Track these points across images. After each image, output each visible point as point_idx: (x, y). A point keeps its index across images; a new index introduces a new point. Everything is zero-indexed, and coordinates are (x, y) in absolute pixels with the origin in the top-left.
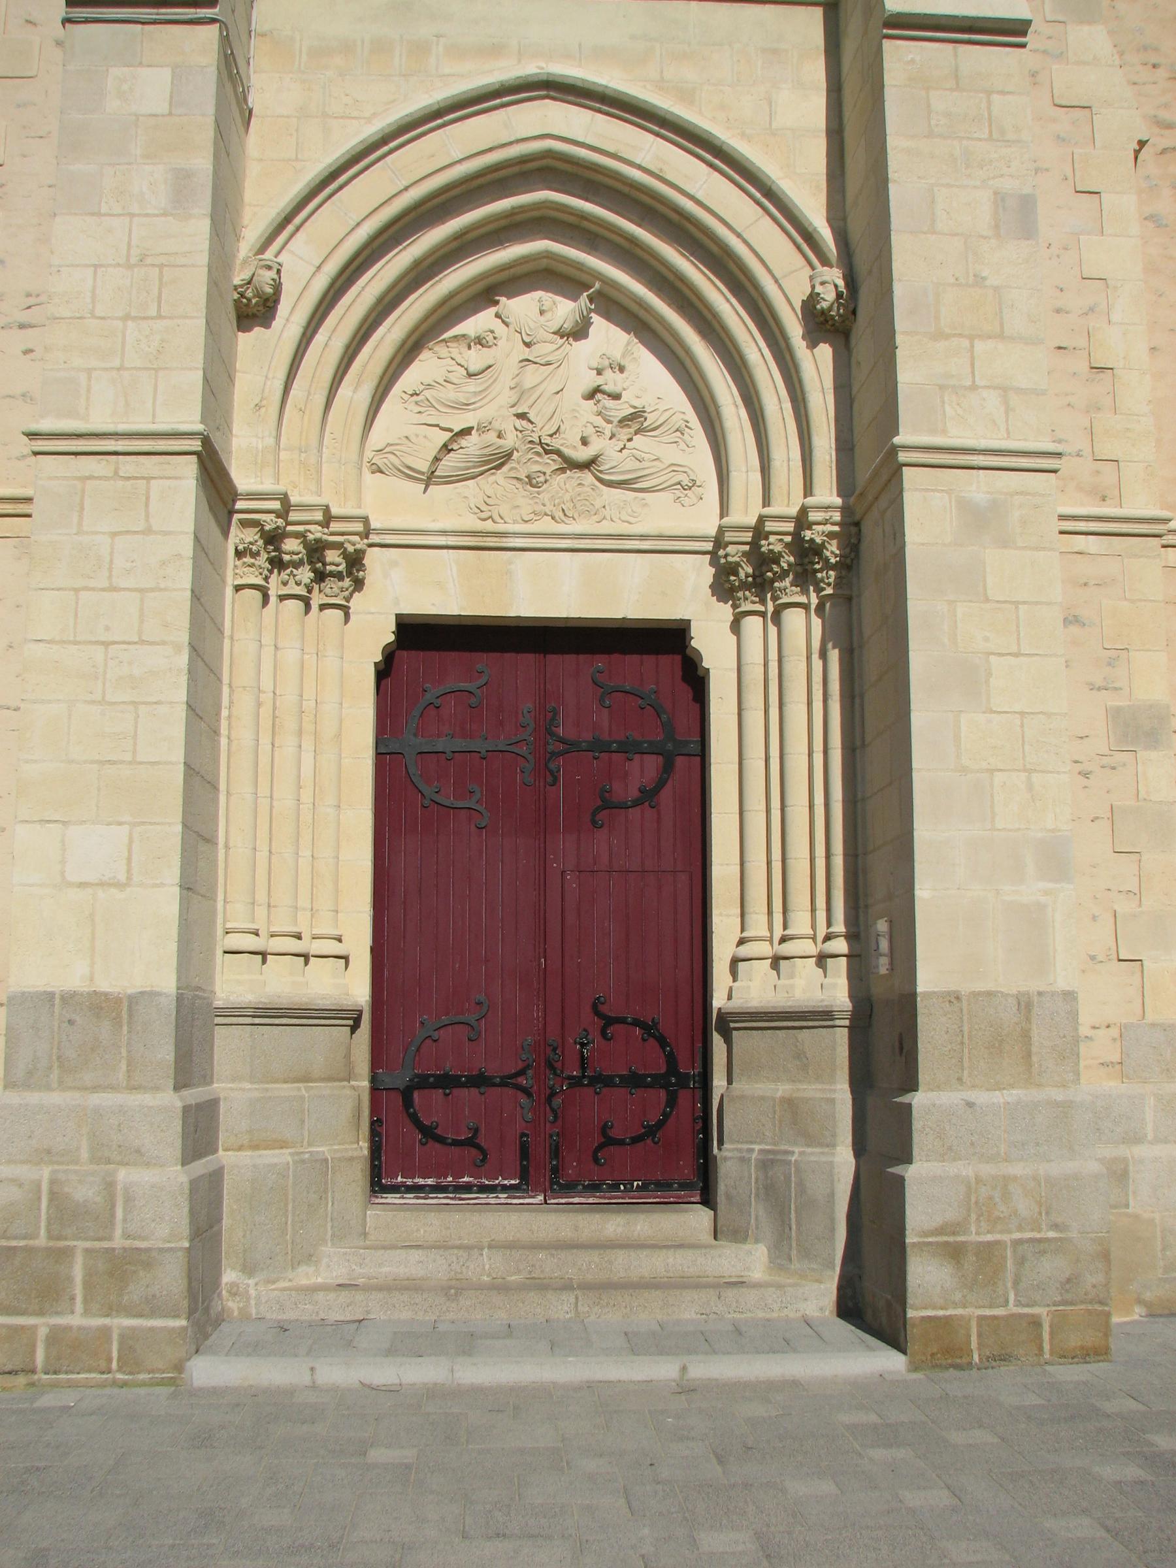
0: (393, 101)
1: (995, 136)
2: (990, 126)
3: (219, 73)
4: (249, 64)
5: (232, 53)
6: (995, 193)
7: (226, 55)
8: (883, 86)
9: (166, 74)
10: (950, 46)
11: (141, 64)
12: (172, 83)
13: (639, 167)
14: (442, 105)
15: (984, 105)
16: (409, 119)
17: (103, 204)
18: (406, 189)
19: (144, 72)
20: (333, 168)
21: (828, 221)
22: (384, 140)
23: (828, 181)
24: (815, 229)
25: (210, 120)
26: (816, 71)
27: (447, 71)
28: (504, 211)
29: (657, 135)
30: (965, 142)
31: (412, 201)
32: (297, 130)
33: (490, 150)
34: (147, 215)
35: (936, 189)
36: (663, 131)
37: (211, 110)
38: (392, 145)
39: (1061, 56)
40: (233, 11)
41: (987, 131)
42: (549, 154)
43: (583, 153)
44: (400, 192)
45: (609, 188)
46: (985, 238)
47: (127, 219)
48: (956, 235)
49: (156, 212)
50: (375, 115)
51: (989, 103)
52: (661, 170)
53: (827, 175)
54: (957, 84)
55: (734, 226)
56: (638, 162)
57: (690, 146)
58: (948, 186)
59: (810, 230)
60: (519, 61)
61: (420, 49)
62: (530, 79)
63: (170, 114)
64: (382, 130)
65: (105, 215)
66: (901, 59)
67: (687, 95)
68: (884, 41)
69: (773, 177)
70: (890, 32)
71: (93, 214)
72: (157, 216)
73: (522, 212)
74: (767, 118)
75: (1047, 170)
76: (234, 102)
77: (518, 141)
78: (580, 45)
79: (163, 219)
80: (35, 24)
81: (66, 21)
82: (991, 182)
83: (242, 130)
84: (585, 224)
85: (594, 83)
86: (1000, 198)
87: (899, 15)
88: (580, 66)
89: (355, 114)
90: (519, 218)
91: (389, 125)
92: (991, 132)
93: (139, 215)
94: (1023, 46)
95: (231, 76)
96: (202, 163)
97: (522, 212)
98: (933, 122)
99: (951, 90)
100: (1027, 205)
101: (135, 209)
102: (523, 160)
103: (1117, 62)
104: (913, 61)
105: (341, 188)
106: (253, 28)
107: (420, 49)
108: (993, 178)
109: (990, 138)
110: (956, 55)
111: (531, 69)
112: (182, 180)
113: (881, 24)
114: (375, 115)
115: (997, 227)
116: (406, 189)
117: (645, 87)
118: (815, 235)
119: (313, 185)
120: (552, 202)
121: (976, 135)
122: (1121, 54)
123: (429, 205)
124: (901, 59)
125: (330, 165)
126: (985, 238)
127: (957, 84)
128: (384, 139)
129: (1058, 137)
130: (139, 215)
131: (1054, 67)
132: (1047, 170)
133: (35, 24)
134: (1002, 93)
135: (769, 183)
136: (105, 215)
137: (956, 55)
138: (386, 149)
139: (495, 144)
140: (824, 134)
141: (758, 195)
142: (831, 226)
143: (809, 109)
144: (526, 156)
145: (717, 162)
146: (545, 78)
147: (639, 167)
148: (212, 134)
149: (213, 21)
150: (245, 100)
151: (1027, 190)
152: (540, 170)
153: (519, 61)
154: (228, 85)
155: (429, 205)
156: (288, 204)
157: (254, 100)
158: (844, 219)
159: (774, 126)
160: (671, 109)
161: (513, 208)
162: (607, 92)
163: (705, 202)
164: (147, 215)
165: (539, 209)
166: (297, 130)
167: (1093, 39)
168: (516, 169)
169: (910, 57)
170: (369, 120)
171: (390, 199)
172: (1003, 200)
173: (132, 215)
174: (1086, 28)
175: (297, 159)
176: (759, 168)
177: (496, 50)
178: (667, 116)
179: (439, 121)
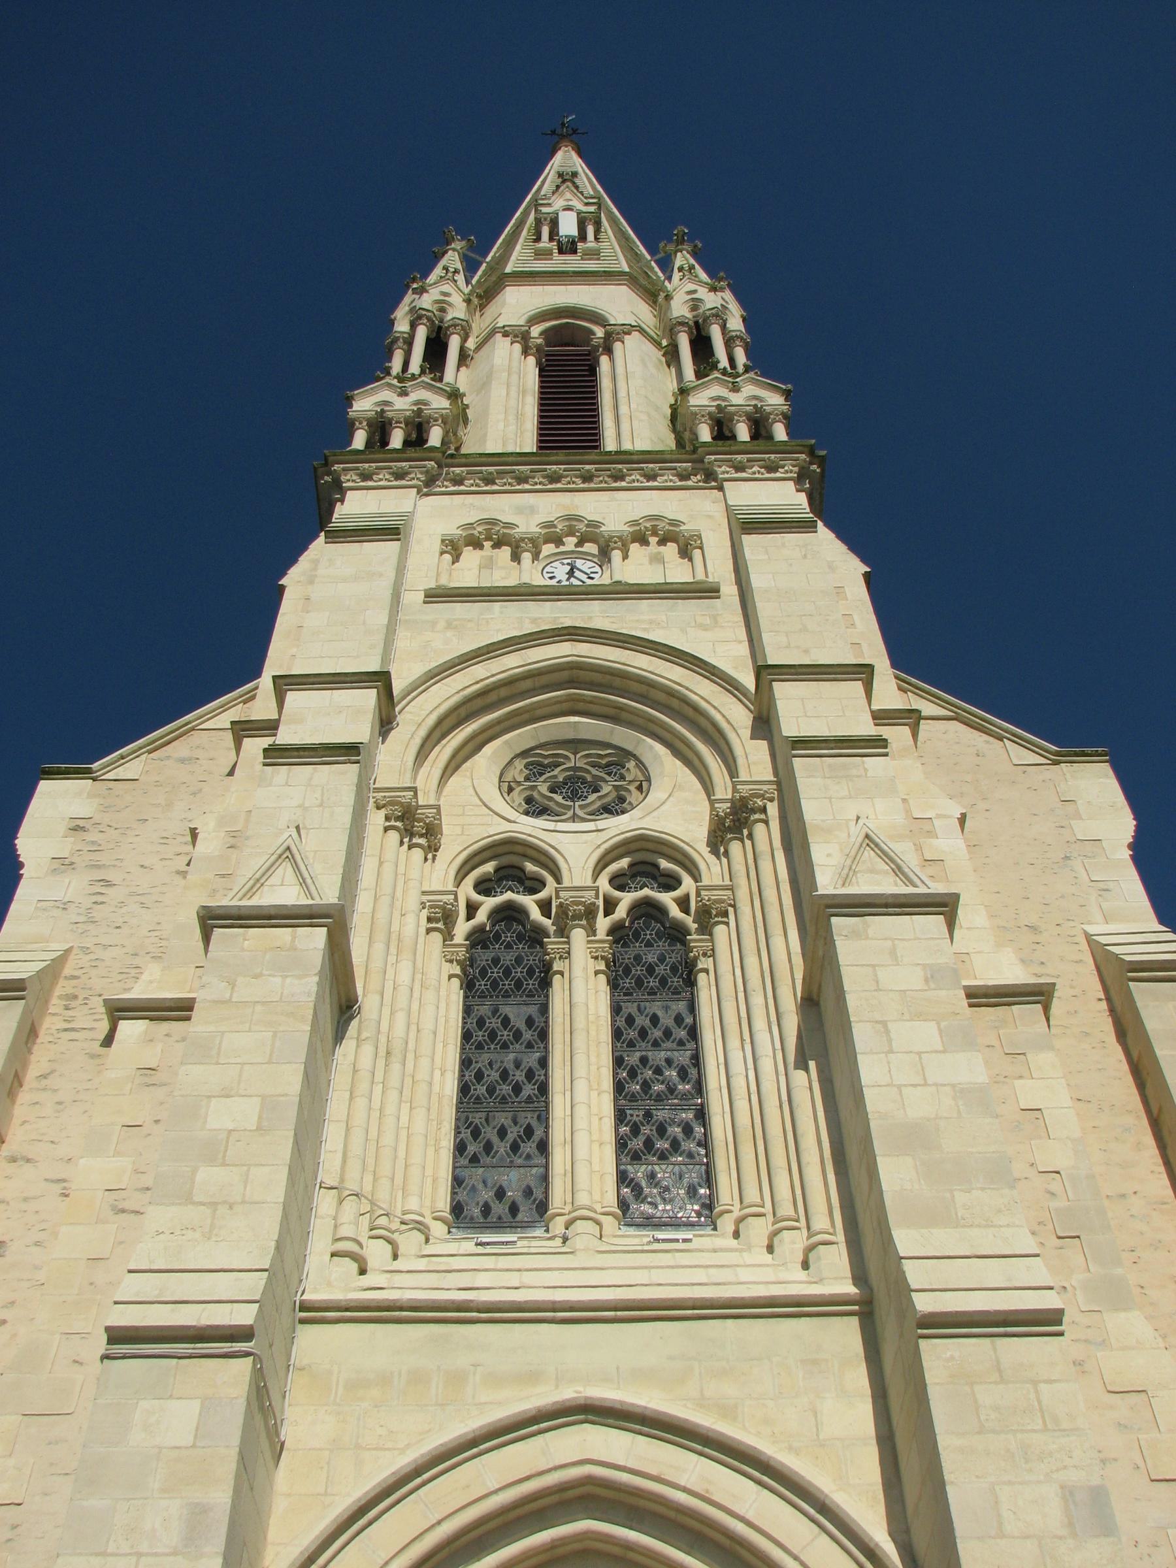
0: (430, 1430)
1: (1050, 1426)
2: (1043, 1417)
3: (249, 1403)
4: (284, 1397)
5: (265, 1385)
6: (1062, 1487)
7: (258, 1387)
8: (925, 1385)
9: (196, 1405)
10: (987, 1340)
11: (171, 1397)
12: (200, 1414)
13: (685, 1490)
14: (478, 1433)
15: (1032, 1396)
16: (443, 1449)
17: (111, 1542)
18: (439, 1523)
19: (174, 1404)
20: (363, 1502)
21: (890, 1535)
22: (417, 1471)
23: (884, 1491)
24: (877, 1545)
25: (234, 1453)
26: (859, 1378)
27: (483, 1399)
28: (543, 1545)
29: (701, 1454)
30: (1019, 1436)
31: (445, 1536)
32: (328, 1463)
33: (528, 1478)
34: (156, 1554)
35: (997, 1488)
36: (707, 1450)
37: (236, 1440)
38: (426, 1476)
39: (1104, 1344)
40: (271, 1346)
41: (1040, 1422)
42: (589, 1480)
43: (624, 1477)
44: (433, 1526)
45: (655, 1515)
46: (1060, 1538)
47: (134, 1559)
48: (1027, 1537)
49: (167, 1550)
50: (408, 1446)
51: (1037, 1392)
52: (707, 1491)
53: (884, 1484)
54: (1001, 1376)
55: (790, 1547)
56: (683, 1483)
57: (736, 1463)
58: (1010, 1483)
59: (872, 1545)
60: (557, 1387)
61: (457, 1379)
62: (567, 1404)
63: (194, 1446)
64: (415, 1460)
65: (112, 1555)
66: (940, 1358)
67: (729, 1411)
68: (920, 1341)
69: (826, 1490)
70: (925, 1331)
71: (97, 1554)
72: (167, 1555)
73: (563, 1545)
74: (814, 1429)
75: (1115, 1460)
76: (263, 1435)
77: (556, 1468)
78: (618, 1368)
79: (171, 1558)
80: (81, 1364)
81: (105, 1357)
82: (1055, 1476)
83: (271, 1464)
84: (631, 1555)
85: (633, 1404)
86: (1068, 1493)
87: (932, 1315)
88: (618, 1388)
89: (389, 1445)
90: (560, 1551)
91: (422, 1455)
92: (1044, 1422)
93: (147, 1554)
94: (1061, 1334)
95: (262, 1408)
96: (221, 1497)
97: (563, 1545)
98: (982, 1418)
99: (996, 1383)
100: (1098, 1497)
101: (144, 1547)
102: (562, 1488)
103: (1162, 1345)
104: (952, 1358)
105: (370, 1523)
106: (292, 1362)
107: (457, 1379)
108: (1057, 1470)
109: (1045, 1429)
110: (995, 1350)
111: (568, 1393)
112: (198, 1514)
113: (914, 1324)
114: (408, 1446)
115: (1071, 1524)
116: (439, 1523)
117: (685, 1406)
118: (877, 1552)
119: (340, 1520)
120: (593, 1532)
121: (1029, 1427)
122: (1164, 1337)
123: (464, 1540)
124: (940, 1358)
125: (359, 1500)
126: (1060, 1538)
127: (1001, 1376)
128: (418, 1471)
129: (1120, 1424)
130: (147, 1554)
131: (1099, 1354)
132: (1115, 1460)
133: (81, 1364)
134: (1050, 1382)
135: (822, 1497)
136: (112, 1555)
137: (995, 1350)
138: (418, 1481)
139: (533, 1472)
140: (874, 1442)
141: (812, 1511)
142: (894, 1540)
143: (856, 1416)
144: (566, 1483)
145: (765, 1479)
146: (582, 1402)
147: (685, 1490)
148: (234, 1466)
149: (247, 1354)
150: (278, 1434)
151: (1095, 1481)
152: (581, 1498)
153: (557, 1387)
154: (258, 1417)
155: (464, 1540)
156: (312, 1542)
157: (288, 1433)
158: (907, 1531)
159: (821, 1437)
160: (775, 1455)
161: (553, 1541)
162: (647, 1413)
163: (756, 1522)
164: (156, 1554)
165: (581, 1541)
166: (328, 1463)
167: (1132, 1324)
168: (555, 1498)
169: (949, 1354)
170: (402, 1451)
171: (422, 1534)
172: (1071, 1494)
173: (140, 1555)
174: (1123, 1315)
175: (326, 1494)
176: (809, 1482)
177: (533, 1377)
178: (710, 1434)
179: (475, 1450)
